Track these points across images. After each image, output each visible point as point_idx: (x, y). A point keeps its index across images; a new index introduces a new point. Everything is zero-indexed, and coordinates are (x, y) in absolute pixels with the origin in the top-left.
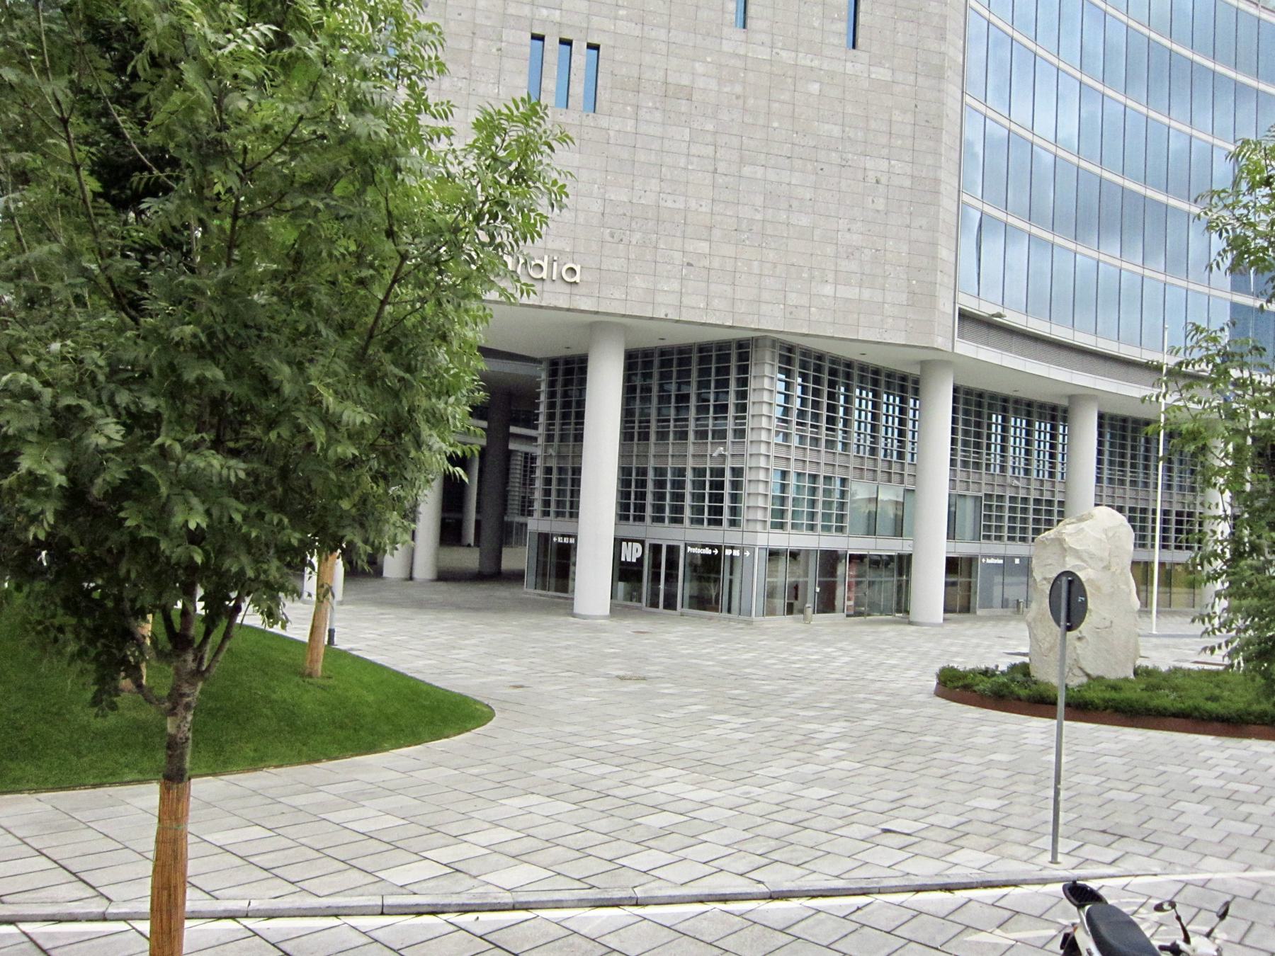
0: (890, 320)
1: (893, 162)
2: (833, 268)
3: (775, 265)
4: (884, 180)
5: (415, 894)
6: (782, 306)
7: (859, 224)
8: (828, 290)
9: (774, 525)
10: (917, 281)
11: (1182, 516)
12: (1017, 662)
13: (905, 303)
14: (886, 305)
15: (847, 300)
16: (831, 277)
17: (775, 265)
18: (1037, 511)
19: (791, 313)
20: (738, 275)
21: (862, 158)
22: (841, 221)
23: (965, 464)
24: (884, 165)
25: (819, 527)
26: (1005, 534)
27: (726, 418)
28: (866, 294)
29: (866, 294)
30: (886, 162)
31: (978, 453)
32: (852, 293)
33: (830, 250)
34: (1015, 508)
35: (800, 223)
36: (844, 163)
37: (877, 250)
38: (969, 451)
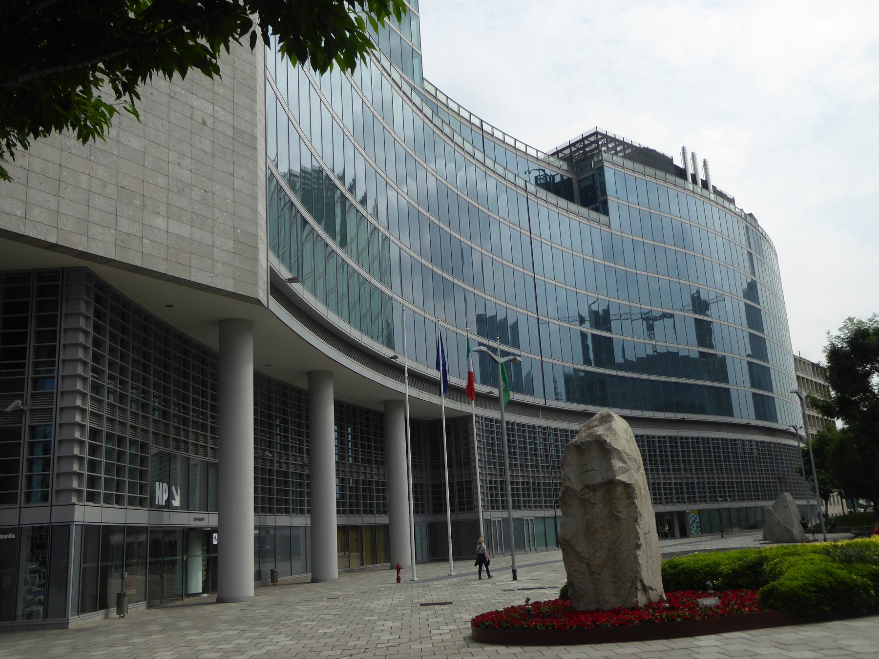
0: (220, 266)
1: (216, 108)
2: (165, 200)
3: (105, 184)
4: (209, 123)
5: (715, 646)
6: (113, 231)
7: (189, 161)
8: (160, 222)
9: (492, 508)
10: (241, 230)
11: (688, 485)
12: (543, 600)
13: (232, 250)
14: (215, 249)
15: (179, 237)
16: (163, 209)
17: (105, 184)
18: (687, 488)
19: (123, 241)
20: (63, 186)
21: (189, 95)
22: (171, 153)
23: (652, 470)
24: (208, 108)
25: (664, 503)
26: (675, 501)
27: (23, 365)
28: (198, 234)
29: (198, 234)
30: (211, 106)
31: (668, 464)
32: (184, 230)
33: (161, 180)
34: (710, 487)
35: (131, 144)
36: (172, 95)
37: (205, 191)
38: (686, 464)
